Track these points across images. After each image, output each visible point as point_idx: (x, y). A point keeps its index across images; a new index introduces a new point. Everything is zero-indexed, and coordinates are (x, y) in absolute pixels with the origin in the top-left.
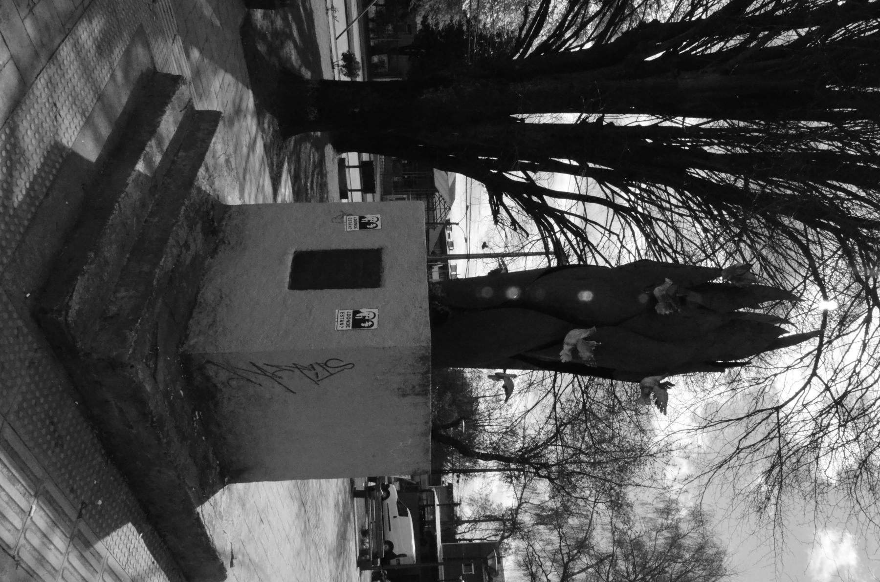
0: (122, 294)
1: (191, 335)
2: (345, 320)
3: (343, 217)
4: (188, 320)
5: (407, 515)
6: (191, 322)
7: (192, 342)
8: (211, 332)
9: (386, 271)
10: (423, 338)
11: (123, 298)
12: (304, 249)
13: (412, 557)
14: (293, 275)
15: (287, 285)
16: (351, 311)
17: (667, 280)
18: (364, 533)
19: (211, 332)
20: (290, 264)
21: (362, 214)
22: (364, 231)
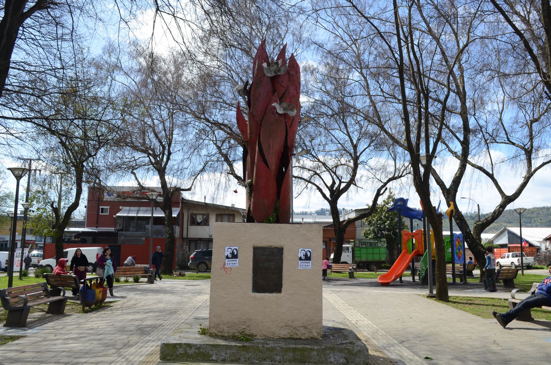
0: (332, 360)
1: (311, 336)
2: (305, 264)
3: (227, 268)
4: (302, 339)
5: (67, 252)
6: (303, 338)
7: (316, 335)
8: (310, 327)
9: (271, 244)
10: (318, 228)
11: (335, 358)
12: (252, 288)
13: (99, 249)
14: (271, 291)
15: (279, 294)
16: (300, 261)
17: (273, 105)
18: (136, 280)
19: (310, 327)
20: (262, 295)
21: (224, 257)
22: (239, 255)
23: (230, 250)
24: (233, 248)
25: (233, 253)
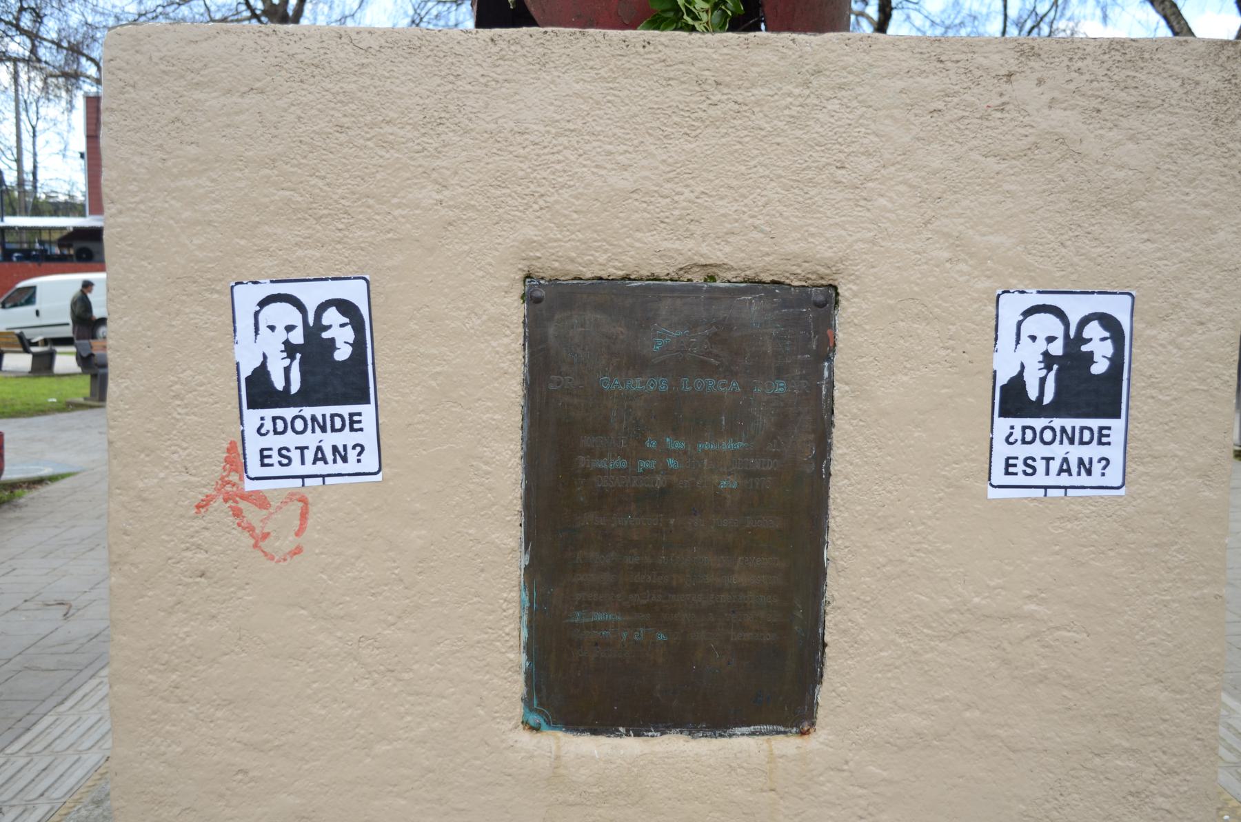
23: (1052, 325)
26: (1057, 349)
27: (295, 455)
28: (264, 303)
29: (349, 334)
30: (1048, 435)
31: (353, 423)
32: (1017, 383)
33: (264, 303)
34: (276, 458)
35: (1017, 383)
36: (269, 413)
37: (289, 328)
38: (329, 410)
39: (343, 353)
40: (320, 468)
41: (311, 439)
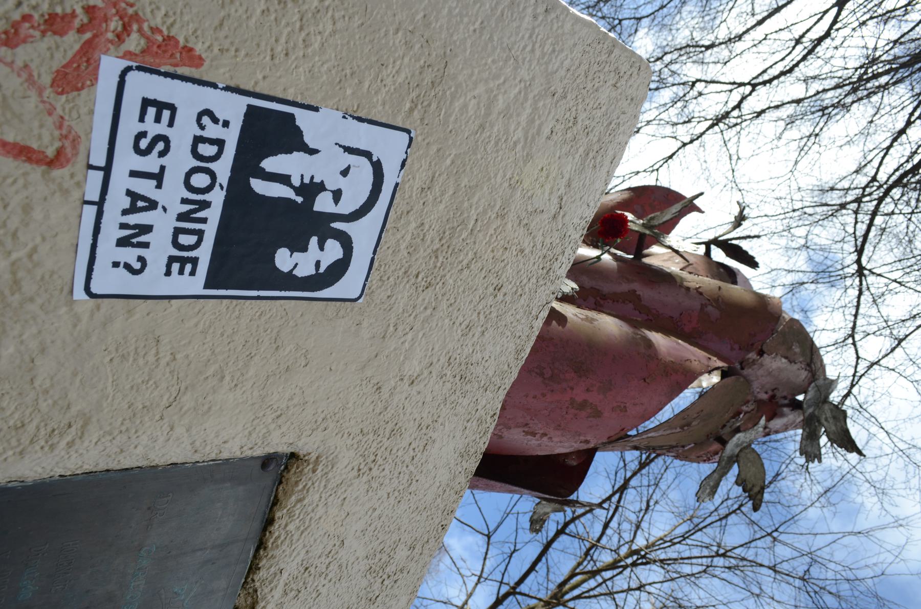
21: (283, 82)
23: (356, 191)
24: (363, 234)
25: (301, 219)
26: (323, 203)
27: (151, 163)
28: (377, 167)
29: (305, 269)
30: (199, 180)
31: (181, 262)
32: (289, 138)
33: (377, 167)
34: (153, 129)
35: (289, 138)
36: (232, 137)
37: (337, 195)
38: (210, 230)
39: (284, 259)
40: (117, 200)
41: (172, 195)
